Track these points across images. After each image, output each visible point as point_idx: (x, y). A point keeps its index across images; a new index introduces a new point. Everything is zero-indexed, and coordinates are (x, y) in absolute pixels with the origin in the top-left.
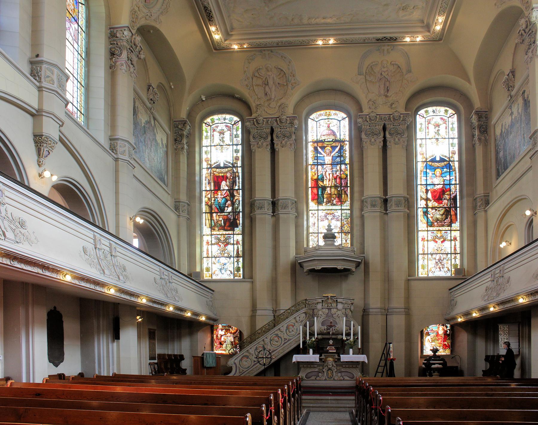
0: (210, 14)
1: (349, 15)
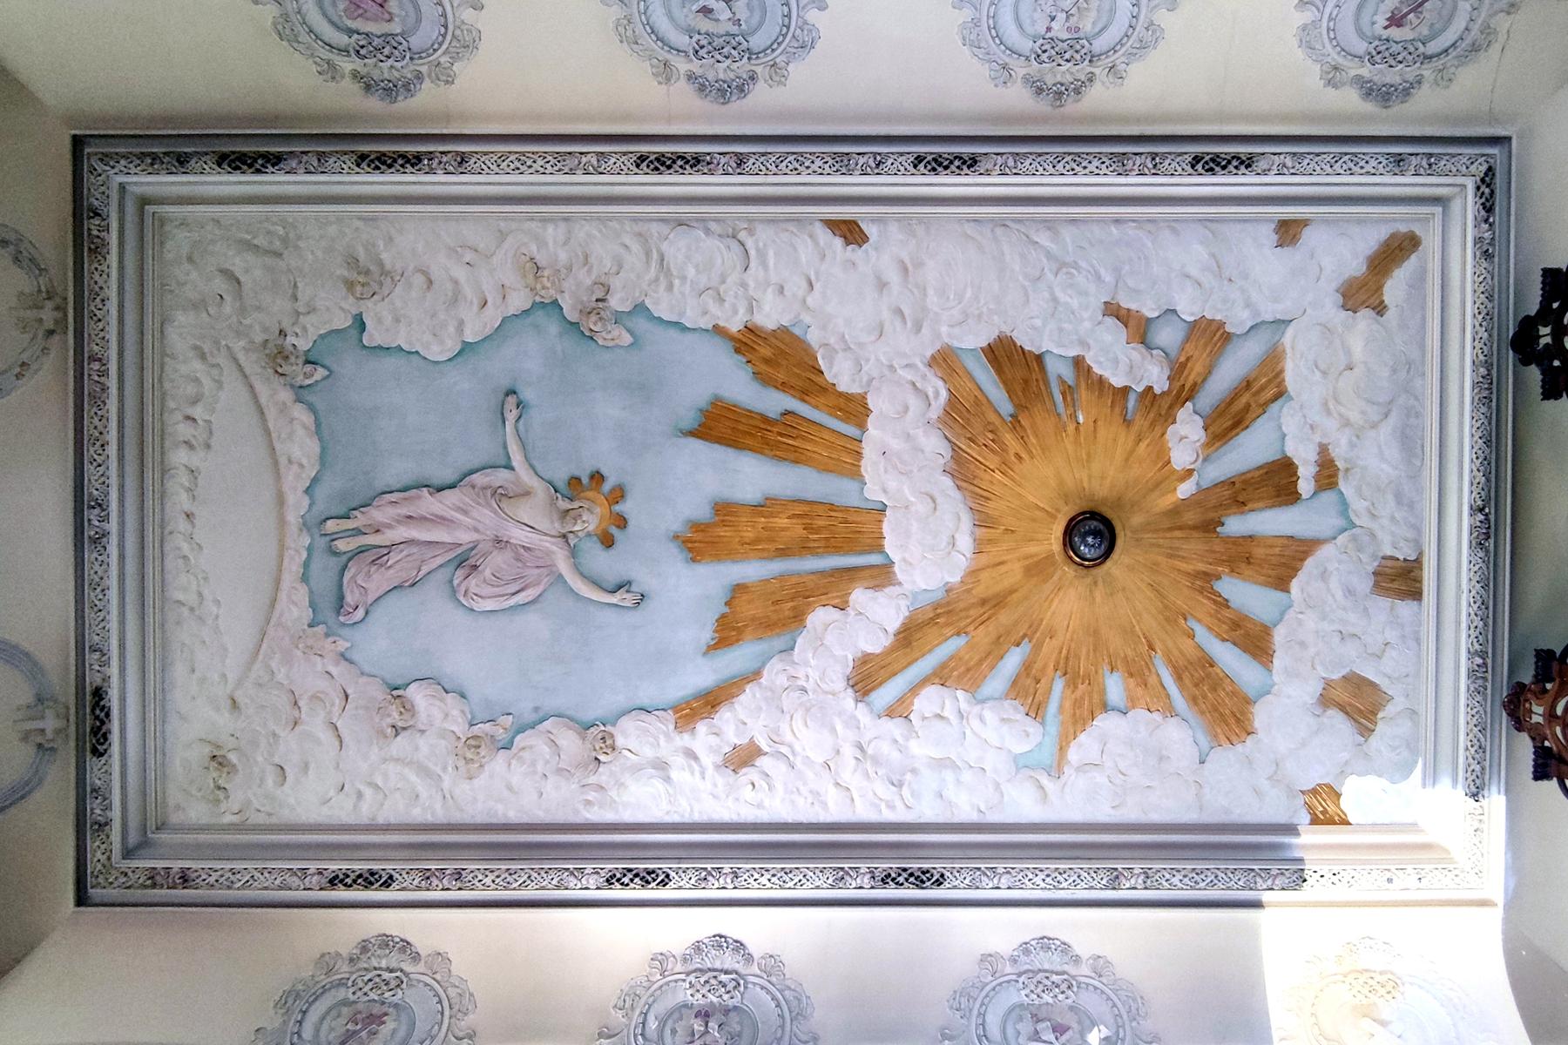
0: (250, 166)
1: (200, 594)
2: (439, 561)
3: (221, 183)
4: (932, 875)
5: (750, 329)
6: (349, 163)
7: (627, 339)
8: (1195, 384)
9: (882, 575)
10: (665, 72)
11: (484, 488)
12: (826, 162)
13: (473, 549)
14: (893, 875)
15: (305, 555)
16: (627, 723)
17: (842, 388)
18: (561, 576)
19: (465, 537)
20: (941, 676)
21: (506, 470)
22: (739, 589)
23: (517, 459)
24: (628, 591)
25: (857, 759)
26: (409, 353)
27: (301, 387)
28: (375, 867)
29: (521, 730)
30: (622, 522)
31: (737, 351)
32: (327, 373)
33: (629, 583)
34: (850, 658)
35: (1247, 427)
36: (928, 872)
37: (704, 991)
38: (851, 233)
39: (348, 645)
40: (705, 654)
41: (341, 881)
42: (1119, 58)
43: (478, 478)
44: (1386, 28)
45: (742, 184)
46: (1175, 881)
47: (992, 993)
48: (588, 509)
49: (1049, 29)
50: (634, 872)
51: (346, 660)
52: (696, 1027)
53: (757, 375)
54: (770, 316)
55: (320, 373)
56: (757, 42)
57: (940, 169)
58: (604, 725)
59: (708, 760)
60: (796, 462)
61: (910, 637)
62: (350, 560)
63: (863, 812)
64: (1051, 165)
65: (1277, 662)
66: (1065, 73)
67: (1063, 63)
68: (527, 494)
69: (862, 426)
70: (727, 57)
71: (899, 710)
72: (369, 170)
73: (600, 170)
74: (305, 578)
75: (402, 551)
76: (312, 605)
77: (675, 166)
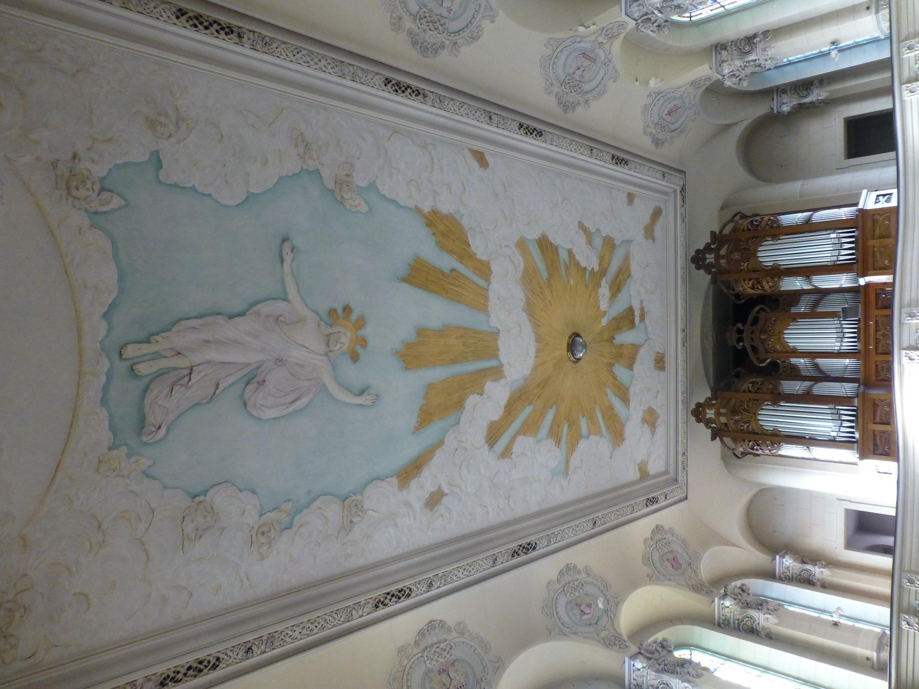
2: (232, 379)
3: (389, 100)
4: (405, 592)
5: (435, 212)
7: (364, 208)
8: (606, 268)
9: (497, 373)
10: (397, 25)
11: (268, 316)
12: (329, 64)
13: (259, 367)
14: (382, 600)
15: (103, 379)
16: (369, 491)
17: (479, 257)
18: (324, 385)
19: (253, 358)
20: (522, 431)
21: (283, 302)
22: (430, 387)
23: (292, 293)
24: (369, 394)
25: (490, 487)
26: (203, 194)
27: (96, 213)
28: (201, 655)
29: (299, 511)
30: (363, 342)
31: (427, 225)
32: (124, 203)
33: (368, 388)
34: (486, 424)
36: (402, 590)
37: (436, 658)
38: (480, 158)
39: (150, 462)
40: (414, 433)
41: (413, 92)
42: (589, 96)
43: (263, 308)
44: (666, 115)
45: (615, 170)
46: (296, 634)
47: (411, 670)
48: (344, 333)
49: (574, 73)
50: (391, 594)
51: (148, 476)
52: (444, 680)
53: (439, 243)
54: (446, 206)
55: (116, 202)
56: (587, 87)
57: (200, 27)
58: (355, 495)
59: (418, 506)
60: (459, 302)
61: (511, 407)
62: (151, 382)
63: (493, 518)
64: (292, 54)
66: (572, 98)
68: (302, 321)
69: (488, 280)
70: (436, 29)
71: (506, 453)
72: (209, 658)
73: (362, 81)
74: (104, 402)
75: (200, 372)
76: (113, 428)
77: (211, 28)
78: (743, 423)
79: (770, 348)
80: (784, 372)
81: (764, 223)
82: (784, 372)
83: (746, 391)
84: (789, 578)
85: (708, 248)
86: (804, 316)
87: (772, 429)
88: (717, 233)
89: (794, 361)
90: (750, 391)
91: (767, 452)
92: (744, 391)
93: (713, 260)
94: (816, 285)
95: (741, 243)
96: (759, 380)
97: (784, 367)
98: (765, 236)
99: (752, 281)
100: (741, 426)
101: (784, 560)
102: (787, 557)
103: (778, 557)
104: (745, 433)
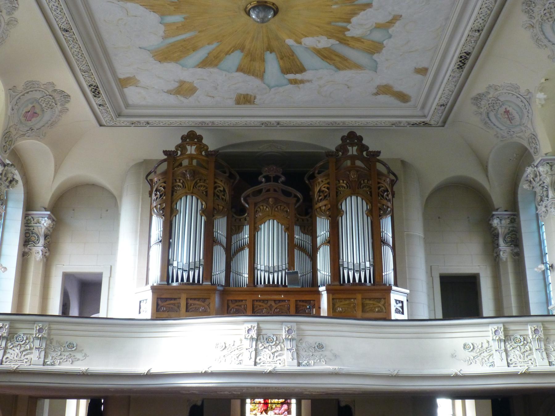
6: (467, 49)
35: (323, 60)
44: (506, 109)
45: (454, 56)
65: (199, 70)
67: (545, 12)
70: (489, 107)
78: (183, 182)
79: (259, 207)
80: (235, 220)
81: (385, 202)
82: (235, 220)
83: (216, 185)
84: (28, 224)
85: (363, 148)
86: (291, 238)
87: (178, 209)
88: (378, 158)
89: (247, 228)
90: (215, 188)
91: (154, 204)
92: (215, 183)
93: (350, 153)
94: (321, 249)
95: (366, 181)
96: (227, 197)
97: (240, 220)
98: (371, 203)
99: (327, 190)
100: (180, 180)
101: (46, 219)
102: (49, 222)
103: (49, 213)
104: (173, 183)
